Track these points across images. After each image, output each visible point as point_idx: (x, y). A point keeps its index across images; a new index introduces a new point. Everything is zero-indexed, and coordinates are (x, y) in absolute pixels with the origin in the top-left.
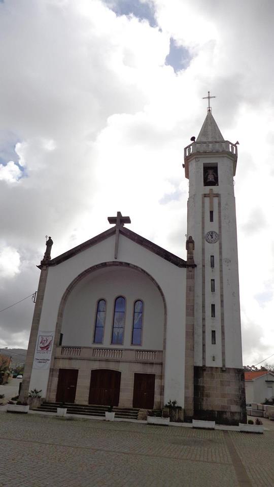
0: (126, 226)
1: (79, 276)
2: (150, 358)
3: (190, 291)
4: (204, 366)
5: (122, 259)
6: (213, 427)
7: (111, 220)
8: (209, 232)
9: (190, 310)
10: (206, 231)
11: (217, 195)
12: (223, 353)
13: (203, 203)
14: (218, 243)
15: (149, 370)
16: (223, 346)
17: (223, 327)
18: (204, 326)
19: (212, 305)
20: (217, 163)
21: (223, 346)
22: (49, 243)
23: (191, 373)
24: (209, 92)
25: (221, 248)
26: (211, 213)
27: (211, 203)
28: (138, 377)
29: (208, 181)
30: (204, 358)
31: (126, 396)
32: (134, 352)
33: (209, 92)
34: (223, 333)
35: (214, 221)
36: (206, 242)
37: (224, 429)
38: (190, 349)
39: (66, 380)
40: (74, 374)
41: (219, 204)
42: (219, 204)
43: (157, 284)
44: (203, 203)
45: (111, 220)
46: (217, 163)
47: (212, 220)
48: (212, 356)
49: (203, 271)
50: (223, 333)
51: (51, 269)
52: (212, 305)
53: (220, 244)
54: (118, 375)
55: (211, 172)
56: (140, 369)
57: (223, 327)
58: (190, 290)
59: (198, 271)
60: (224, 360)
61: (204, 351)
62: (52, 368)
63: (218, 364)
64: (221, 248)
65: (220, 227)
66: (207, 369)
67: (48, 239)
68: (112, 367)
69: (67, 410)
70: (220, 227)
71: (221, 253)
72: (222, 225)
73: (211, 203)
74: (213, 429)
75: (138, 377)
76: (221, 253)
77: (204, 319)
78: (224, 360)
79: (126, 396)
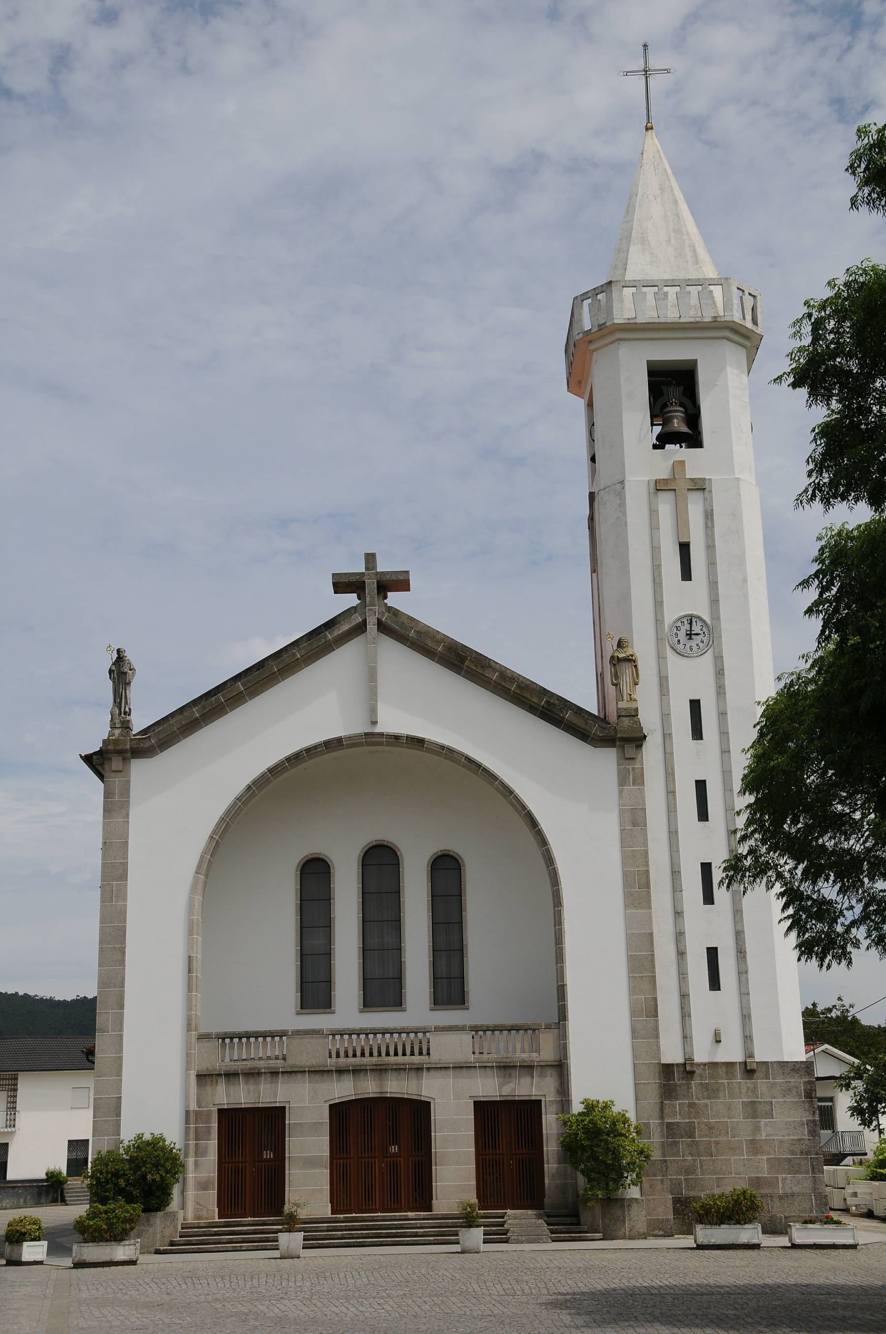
0: (394, 599)
1: (249, 788)
2: (518, 1049)
3: (634, 824)
4: (689, 1060)
5: (393, 721)
6: (755, 1241)
7: (343, 584)
8: (680, 619)
9: (637, 888)
10: (670, 616)
11: (700, 486)
12: (746, 1018)
13: (653, 513)
14: (709, 656)
15: (523, 1088)
16: (744, 994)
17: (739, 935)
18: (680, 936)
19: (692, 701)
20: (695, 362)
21: (744, 994)
22: (120, 672)
23: (653, 1082)
24: (645, 46)
25: (720, 673)
26: (684, 548)
27: (681, 520)
28: (486, 1112)
29: (663, 387)
30: (686, 1037)
31: (455, 1173)
32: (467, 1037)
33: (645, 46)
34: (741, 953)
35: (704, 737)
36: (670, 653)
37: (630, 1241)
38: (645, 1013)
39: (250, 1144)
40: (271, 1123)
41: (709, 516)
42: (709, 516)
43: (524, 807)
44: (653, 513)
45: (343, 584)
46: (695, 362)
47: (715, 983)
48: (642, 43)
49: (668, 755)
50: (741, 953)
51: (139, 769)
52: (692, 701)
53: (718, 659)
54: (420, 1111)
55: (674, 393)
56: (489, 1087)
57: (739, 935)
58: (634, 820)
59: (651, 754)
60: (747, 1038)
61: (685, 1015)
62: (193, 1107)
63: (731, 1052)
64: (720, 673)
65: (714, 601)
66: (698, 1071)
67: (115, 656)
68: (395, 1087)
69: (305, 1239)
70: (714, 601)
71: (720, 691)
72: (722, 589)
73: (681, 520)
74: (756, 1247)
75: (486, 1112)
76: (720, 691)
77: (678, 914)
78: (747, 1038)
79: (455, 1173)
